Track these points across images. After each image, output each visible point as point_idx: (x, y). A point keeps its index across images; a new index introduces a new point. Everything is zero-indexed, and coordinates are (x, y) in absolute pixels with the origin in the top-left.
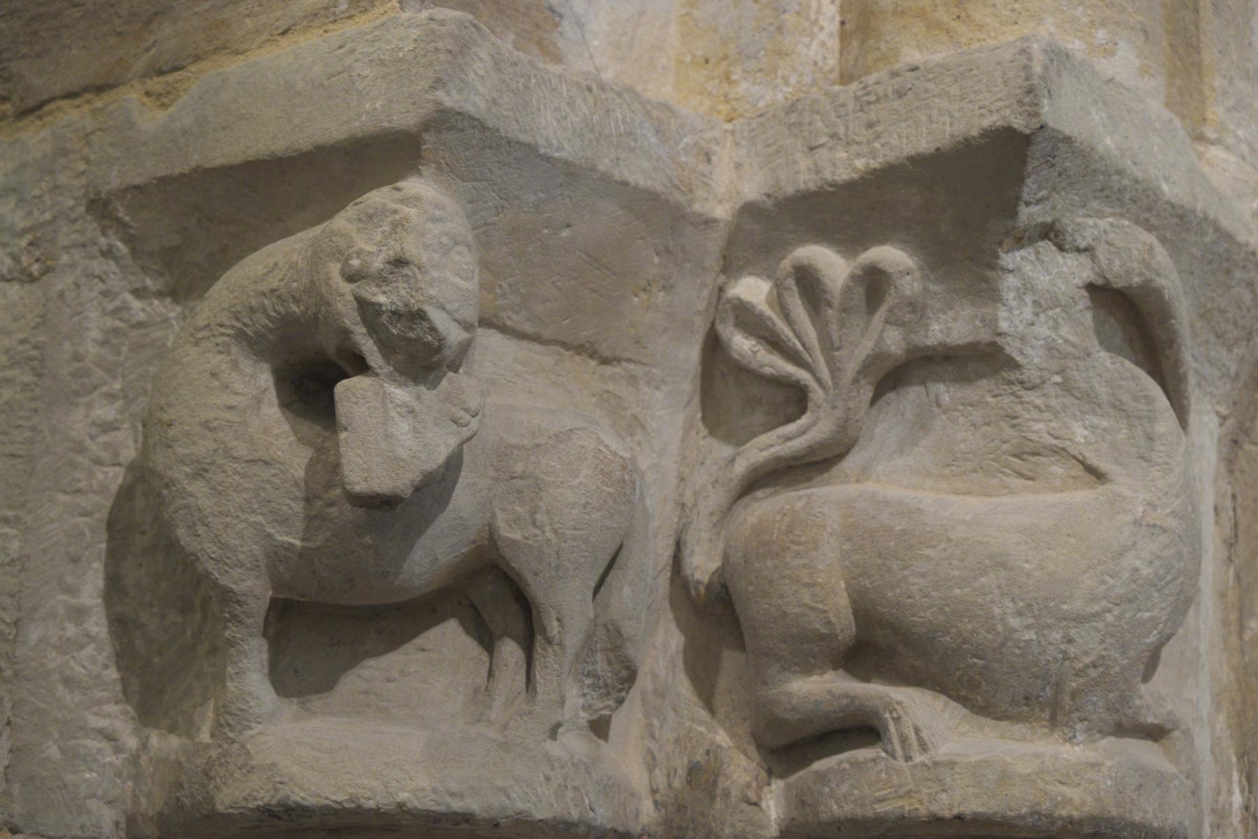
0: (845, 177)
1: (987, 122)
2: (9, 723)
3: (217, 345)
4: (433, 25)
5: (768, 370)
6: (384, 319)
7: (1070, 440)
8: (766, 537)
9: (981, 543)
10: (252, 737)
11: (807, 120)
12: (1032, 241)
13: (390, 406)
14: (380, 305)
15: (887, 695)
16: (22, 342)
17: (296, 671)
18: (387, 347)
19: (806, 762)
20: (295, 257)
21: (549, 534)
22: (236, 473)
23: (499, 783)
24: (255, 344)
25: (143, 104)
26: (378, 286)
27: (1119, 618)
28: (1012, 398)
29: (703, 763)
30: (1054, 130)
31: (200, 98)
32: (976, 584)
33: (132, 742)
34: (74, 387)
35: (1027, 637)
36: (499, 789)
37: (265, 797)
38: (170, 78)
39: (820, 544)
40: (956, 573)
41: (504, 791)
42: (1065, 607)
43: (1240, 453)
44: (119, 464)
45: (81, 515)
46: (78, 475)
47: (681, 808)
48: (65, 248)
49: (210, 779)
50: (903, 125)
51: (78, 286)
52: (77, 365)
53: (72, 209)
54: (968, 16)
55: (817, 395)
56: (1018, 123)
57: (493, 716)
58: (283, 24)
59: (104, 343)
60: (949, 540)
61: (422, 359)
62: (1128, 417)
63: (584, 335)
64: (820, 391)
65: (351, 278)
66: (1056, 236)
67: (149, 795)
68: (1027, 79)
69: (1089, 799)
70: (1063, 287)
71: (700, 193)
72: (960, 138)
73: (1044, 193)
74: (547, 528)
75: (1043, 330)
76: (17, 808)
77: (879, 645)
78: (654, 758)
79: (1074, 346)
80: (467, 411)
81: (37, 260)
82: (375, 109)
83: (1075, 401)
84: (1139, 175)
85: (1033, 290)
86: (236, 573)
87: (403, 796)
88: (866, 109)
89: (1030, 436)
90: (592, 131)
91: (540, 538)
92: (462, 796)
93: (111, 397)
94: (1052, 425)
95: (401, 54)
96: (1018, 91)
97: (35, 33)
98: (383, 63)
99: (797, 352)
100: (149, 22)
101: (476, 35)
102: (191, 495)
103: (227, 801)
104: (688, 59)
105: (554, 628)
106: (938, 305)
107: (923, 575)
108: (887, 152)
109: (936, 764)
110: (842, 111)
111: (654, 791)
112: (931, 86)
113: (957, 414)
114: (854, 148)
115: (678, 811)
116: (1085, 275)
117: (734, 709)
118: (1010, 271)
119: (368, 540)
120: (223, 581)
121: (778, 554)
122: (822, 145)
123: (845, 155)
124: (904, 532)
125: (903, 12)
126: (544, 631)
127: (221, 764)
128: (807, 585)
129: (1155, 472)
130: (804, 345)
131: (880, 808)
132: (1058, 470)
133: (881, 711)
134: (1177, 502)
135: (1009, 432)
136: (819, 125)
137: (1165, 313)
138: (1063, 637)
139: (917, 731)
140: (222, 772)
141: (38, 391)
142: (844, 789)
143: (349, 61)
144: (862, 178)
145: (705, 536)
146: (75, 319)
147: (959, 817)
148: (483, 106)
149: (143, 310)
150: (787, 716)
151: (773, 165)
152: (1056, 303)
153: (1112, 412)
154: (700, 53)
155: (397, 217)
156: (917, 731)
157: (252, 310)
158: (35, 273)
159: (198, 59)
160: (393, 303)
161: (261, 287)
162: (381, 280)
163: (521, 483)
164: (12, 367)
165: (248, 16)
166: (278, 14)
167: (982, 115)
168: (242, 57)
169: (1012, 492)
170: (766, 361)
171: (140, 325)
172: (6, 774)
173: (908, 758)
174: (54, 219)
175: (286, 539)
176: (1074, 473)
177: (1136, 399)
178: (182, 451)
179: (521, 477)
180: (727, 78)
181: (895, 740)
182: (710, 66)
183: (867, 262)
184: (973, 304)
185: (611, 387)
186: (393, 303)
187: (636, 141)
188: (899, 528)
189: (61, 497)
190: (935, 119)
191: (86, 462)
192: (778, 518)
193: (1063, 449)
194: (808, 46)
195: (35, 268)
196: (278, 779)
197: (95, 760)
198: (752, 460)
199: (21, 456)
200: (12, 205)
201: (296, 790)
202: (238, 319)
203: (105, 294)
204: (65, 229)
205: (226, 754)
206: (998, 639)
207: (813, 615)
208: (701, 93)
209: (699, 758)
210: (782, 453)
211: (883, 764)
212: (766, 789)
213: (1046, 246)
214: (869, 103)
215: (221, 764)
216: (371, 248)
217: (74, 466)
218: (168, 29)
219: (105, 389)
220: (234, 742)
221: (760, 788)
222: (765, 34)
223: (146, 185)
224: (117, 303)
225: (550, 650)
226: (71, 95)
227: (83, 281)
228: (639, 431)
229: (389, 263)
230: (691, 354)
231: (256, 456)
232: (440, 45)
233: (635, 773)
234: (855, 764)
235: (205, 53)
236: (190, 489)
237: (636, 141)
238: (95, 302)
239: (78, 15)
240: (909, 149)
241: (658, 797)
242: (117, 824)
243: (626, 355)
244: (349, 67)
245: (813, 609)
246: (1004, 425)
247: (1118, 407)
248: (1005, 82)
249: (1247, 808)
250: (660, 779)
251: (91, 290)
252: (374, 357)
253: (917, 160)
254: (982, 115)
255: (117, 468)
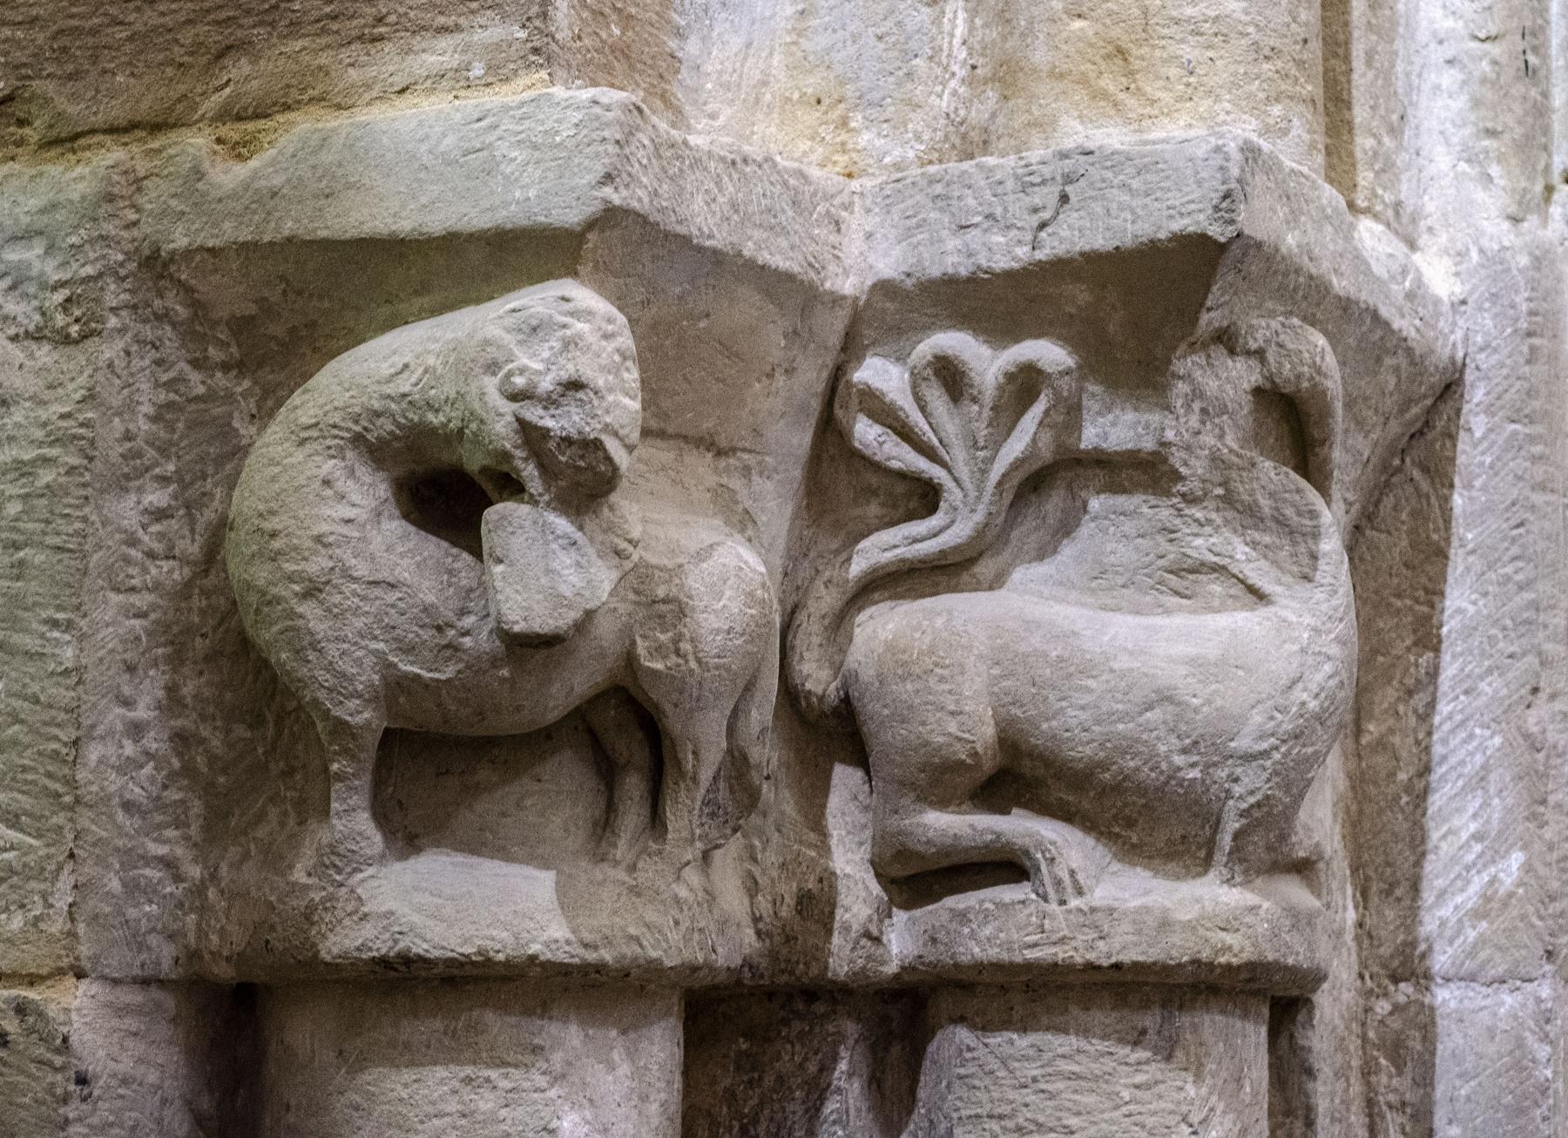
0: (1002, 265)
1: (1177, 226)
2: (72, 856)
3: (329, 448)
4: (597, 110)
5: (895, 464)
6: (552, 445)
7: (1231, 557)
8: (905, 657)
9: (1146, 675)
10: (363, 881)
11: (956, 194)
12: (1205, 346)
13: (551, 537)
14: (548, 430)
15: (1038, 833)
16: (63, 417)
17: (400, 803)
18: (548, 470)
19: (934, 897)
20: (431, 361)
21: (693, 664)
22: (354, 593)
23: (632, 931)
24: (375, 451)
25: (215, 153)
26: (545, 408)
27: (1285, 756)
28: (1172, 511)
29: (815, 891)
30: (1249, 237)
31: (294, 156)
32: (1141, 720)
33: (195, 872)
34: (126, 470)
35: (1191, 776)
36: (631, 937)
37: (382, 948)
38: (250, 126)
39: (949, 658)
40: (1120, 707)
41: (637, 940)
42: (1233, 744)
43: (1361, 540)
44: (174, 557)
45: (136, 616)
46: (131, 571)
47: (789, 939)
48: (112, 309)
49: (313, 924)
50: (1075, 215)
51: (128, 353)
52: (128, 445)
53: (122, 265)
54: (1138, 89)
55: (952, 494)
56: (1218, 232)
57: (619, 855)
58: (399, 81)
59: (155, 419)
60: (1112, 671)
61: (583, 481)
62: (1291, 533)
63: (708, 425)
64: (957, 491)
65: (515, 397)
66: (1230, 339)
67: (222, 932)
68: (1224, 183)
69: (1249, 949)
70: (1231, 392)
71: (832, 268)
72: (1144, 239)
73: (1227, 297)
74: (691, 657)
75: (1209, 439)
76: (84, 950)
77: (1018, 772)
78: (756, 882)
79: (1239, 456)
80: (630, 541)
81: (77, 321)
82: (528, 199)
83: (1236, 515)
84: (1314, 271)
85: (1202, 396)
86: (353, 704)
87: (534, 948)
88: (1029, 190)
89: (1189, 552)
90: (737, 211)
91: (683, 668)
92: (596, 948)
93: (164, 480)
94: (1212, 540)
95: (558, 139)
96: (1213, 195)
97: (64, 50)
98: (535, 147)
99: (932, 448)
100: (220, 56)
101: (639, 121)
102: (301, 616)
103: (335, 951)
104: (796, 96)
105: (689, 762)
106: (1096, 407)
107: (1083, 708)
108: (1056, 243)
109: (1093, 910)
110: (1000, 190)
111: (756, 920)
112: (1109, 175)
113: (1107, 522)
114: (1014, 232)
115: (788, 941)
116: (1253, 379)
117: (849, 833)
118: (1180, 378)
119: (505, 672)
120: (337, 712)
121: (919, 677)
122: (976, 225)
123: (1002, 239)
124: (1060, 659)
125: (1062, 75)
126: (678, 764)
127: (326, 909)
128: (952, 713)
129: (1319, 595)
130: (941, 442)
131: (1031, 955)
132: (1216, 588)
133: (1032, 850)
134: (1341, 626)
135: (1165, 546)
136: (971, 202)
137: (1326, 413)
138: (1229, 776)
139: (1072, 873)
140: (328, 917)
141: (88, 476)
142: (988, 931)
143: (491, 138)
144: (1024, 269)
145: (816, 640)
146: (125, 392)
147: (1117, 966)
148: (646, 200)
149: (203, 383)
150: (920, 848)
151: (915, 240)
152: (1224, 410)
153: (1273, 525)
154: (810, 91)
155: (568, 332)
156: (1072, 873)
157: (378, 414)
158: (75, 335)
159: (287, 108)
160: (563, 428)
161: (389, 389)
162: (549, 402)
163: (664, 608)
164: (51, 444)
165: (352, 65)
166: (391, 68)
167: (1171, 217)
168: (346, 113)
169: (1168, 612)
170: (894, 454)
171: (198, 399)
172: (70, 913)
173: (1062, 902)
174: (101, 275)
175: (409, 668)
176: (1232, 591)
177: (1299, 514)
178: (290, 567)
179: (664, 601)
180: (844, 123)
181: (1047, 881)
182: (823, 108)
183: (1023, 359)
184: (1136, 409)
185: (724, 481)
186: (563, 428)
187: (775, 216)
188: (1054, 654)
189: (115, 598)
190: (1114, 212)
191: (140, 555)
192: (917, 635)
193: (1224, 568)
194: (940, 96)
195: (74, 330)
196: (397, 929)
197: (155, 891)
198: (873, 561)
199: (71, 551)
200: (39, 251)
201: (418, 941)
202: (356, 422)
203: (158, 363)
204: (113, 287)
205: (331, 898)
206: (1162, 778)
207: (958, 746)
208: (812, 139)
209: (810, 886)
210: (909, 555)
211: (1033, 907)
212: (887, 922)
213: (1218, 352)
214: (1033, 185)
215: (326, 909)
216: (536, 365)
217: (127, 560)
218: (245, 67)
219: (157, 470)
220: (341, 885)
221: (881, 921)
222: (892, 79)
223: (222, 249)
224: (171, 374)
225: (682, 785)
226: (112, 130)
227: (134, 348)
228: (750, 526)
229: (560, 384)
230: (802, 439)
231: (379, 577)
232: (606, 134)
233: (733, 901)
234: (999, 905)
235: (299, 102)
236: (300, 610)
237: (775, 216)
238: (147, 372)
239: (123, 35)
240: (1082, 245)
241: (761, 925)
242: (177, 960)
243: (740, 445)
244: (490, 144)
245: (959, 739)
246: (1160, 539)
247: (1281, 522)
248: (1199, 183)
249: (1360, 925)
250: (764, 905)
251: (142, 358)
252: (535, 484)
253: (1092, 259)
254: (1171, 217)
255: (171, 562)
